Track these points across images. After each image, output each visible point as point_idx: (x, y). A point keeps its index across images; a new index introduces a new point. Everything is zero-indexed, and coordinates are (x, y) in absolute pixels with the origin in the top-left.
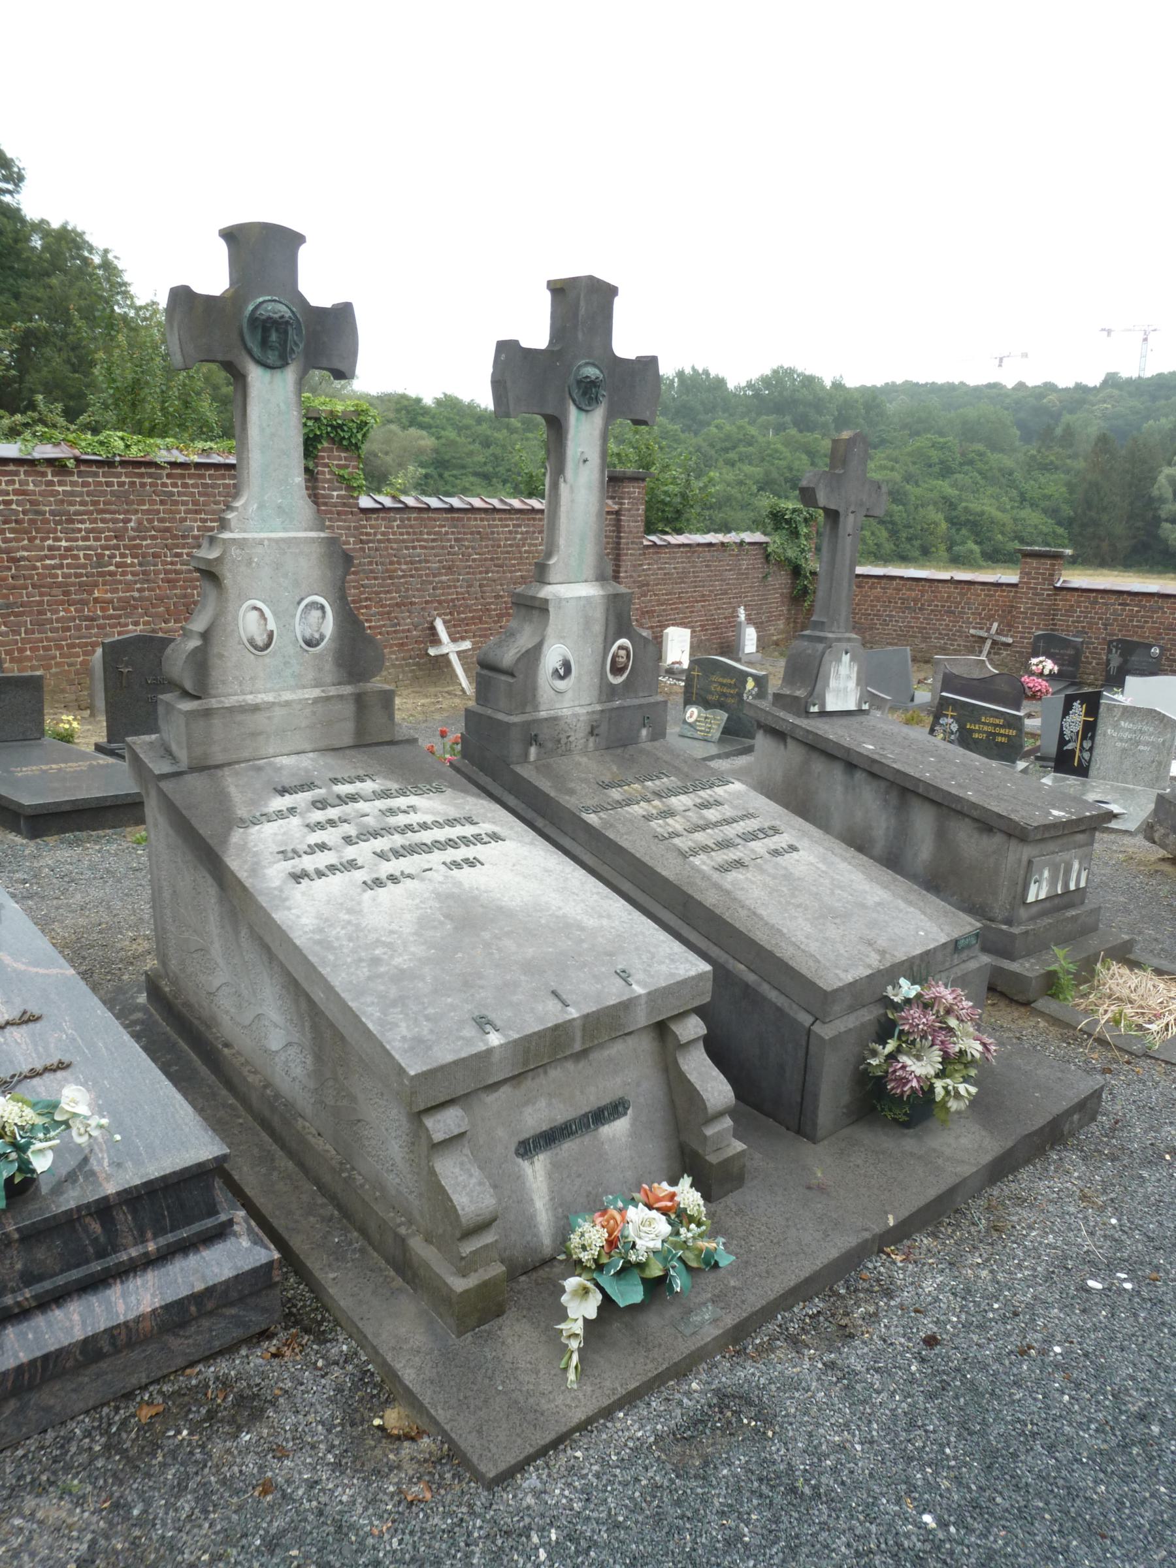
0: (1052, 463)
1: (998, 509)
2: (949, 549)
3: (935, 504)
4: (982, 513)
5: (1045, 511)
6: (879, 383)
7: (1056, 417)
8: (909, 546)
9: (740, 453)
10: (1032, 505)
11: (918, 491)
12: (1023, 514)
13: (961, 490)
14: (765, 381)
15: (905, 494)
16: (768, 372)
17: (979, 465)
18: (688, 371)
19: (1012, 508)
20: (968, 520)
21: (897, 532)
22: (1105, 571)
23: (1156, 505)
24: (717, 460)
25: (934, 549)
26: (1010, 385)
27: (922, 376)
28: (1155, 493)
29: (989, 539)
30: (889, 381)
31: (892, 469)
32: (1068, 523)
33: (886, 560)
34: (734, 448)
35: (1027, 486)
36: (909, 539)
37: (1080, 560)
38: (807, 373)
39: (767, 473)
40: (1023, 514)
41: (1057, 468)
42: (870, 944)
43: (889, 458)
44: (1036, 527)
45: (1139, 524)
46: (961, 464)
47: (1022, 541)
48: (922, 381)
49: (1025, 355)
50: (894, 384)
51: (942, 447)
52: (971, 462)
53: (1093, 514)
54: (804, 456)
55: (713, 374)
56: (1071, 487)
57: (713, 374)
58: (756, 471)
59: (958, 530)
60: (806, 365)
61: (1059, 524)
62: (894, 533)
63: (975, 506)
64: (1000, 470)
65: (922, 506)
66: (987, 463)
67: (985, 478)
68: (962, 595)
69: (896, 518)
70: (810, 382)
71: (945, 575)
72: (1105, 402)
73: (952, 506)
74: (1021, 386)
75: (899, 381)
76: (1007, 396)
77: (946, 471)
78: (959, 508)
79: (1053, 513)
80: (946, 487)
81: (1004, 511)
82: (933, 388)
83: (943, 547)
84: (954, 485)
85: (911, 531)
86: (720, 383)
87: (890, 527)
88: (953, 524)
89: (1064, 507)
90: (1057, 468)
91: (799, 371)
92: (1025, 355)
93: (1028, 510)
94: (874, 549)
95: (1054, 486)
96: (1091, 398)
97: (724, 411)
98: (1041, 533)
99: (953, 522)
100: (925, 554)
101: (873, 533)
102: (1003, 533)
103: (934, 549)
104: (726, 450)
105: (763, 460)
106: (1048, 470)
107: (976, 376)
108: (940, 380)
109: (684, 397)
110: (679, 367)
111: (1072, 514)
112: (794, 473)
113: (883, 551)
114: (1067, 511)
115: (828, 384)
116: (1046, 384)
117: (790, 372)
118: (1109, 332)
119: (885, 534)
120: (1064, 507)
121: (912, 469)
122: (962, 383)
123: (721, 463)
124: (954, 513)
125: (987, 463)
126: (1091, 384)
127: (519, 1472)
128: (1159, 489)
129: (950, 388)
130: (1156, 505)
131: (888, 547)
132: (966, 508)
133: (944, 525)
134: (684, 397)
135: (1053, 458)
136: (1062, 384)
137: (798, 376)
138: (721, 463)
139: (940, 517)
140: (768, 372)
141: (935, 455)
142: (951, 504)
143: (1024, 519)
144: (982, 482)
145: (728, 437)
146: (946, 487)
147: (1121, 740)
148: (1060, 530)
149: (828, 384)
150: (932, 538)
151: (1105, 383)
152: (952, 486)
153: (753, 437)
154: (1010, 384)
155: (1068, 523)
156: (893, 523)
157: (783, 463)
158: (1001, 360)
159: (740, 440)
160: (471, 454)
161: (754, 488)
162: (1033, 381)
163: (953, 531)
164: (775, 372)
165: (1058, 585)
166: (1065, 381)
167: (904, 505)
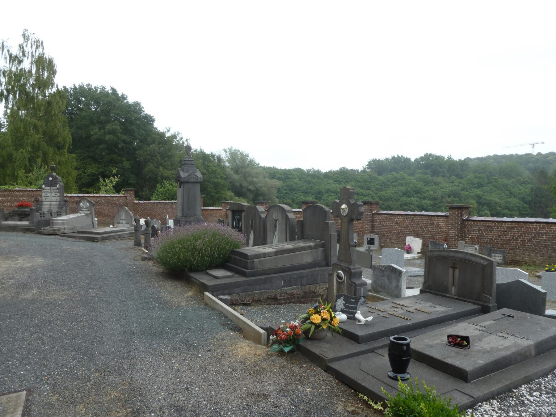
0: (527, 181)
1: (499, 198)
4: (492, 200)
5: (520, 199)
12: (510, 200)
14: (422, 158)
17: (494, 183)
18: (396, 156)
27: (500, 152)
29: (495, 209)
32: (529, 203)
42: (206, 304)
44: (515, 204)
46: (487, 183)
47: (509, 209)
49: (543, 143)
50: (489, 156)
52: (491, 182)
57: (234, 149)
59: (482, 207)
60: (496, 154)
61: (525, 203)
70: (438, 158)
73: (480, 198)
74: (539, 154)
75: (492, 155)
77: (480, 186)
79: (523, 199)
90: (529, 183)
92: (543, 143)
95: (525, 190)
98: (517, 206)
102: (500, 207)
104: (395, 182)
107: (522, 151)
117: (430, 155)
120: (526, 197)
123: (391, 186)
124: (481, 200)
127: (470, 408)
132: (485, 199)
138: (391, 186)
146: (478, 192)
148: (525, 205)
149: (446, 158)
155: (529, 203)
158: (533, 145)
160: (303, 186)
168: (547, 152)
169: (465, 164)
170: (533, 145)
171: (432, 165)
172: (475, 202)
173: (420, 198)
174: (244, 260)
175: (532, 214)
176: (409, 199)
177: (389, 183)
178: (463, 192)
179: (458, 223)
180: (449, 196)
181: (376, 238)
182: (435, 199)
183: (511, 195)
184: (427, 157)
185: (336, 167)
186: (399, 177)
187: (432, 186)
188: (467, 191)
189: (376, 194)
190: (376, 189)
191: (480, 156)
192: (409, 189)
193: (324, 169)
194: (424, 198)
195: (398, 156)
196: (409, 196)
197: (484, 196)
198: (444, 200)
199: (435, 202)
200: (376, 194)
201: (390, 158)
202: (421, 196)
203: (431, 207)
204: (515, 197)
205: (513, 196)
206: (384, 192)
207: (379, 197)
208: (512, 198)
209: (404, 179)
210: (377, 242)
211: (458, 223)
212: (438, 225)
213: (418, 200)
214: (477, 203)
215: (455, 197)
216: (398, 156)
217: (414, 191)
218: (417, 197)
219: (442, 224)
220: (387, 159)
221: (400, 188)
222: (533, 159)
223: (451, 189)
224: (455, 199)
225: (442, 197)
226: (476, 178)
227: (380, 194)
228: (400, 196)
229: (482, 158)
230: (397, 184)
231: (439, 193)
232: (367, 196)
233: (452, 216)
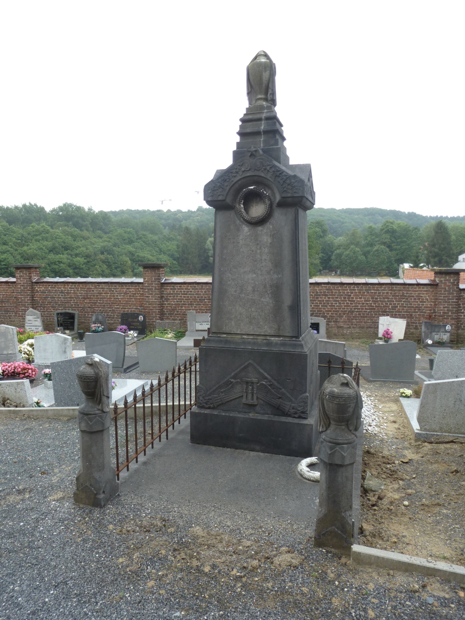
0: (172, 238)
2: (133, 271)
3: (126, 254)
4: (144, 257)
5: (169, 255)
6: (117, 210)
7: (180, 221)
8: (116, 271)
9: (43, 237)
10: (164, 253)
11: (119, 250)
12: (161, 257)
13: (136, 248)
14: (61, 209)
15: (113, 250)
16: (62, 205)
17: (144, 239)
18: (28, 204)
19: (157, 254)
20: (139, 260)
21: (111, 266)
22: (192, 276)
23: (207, 251)
24: (32, 240)
25: (126, 271)
26: (165, 211)
28: (206, 247)
30: (121, 209)
31: (109, 242)
33: (106, 276)
34: (40, 234)
35: (162, 246)
36: (116, 268)
37: (183, 272)
38: (78, 205)
39: (54, 244)
40: (161, 257)
41: (173, 240)
43: (108, 237)
45: (203, 258)
46: (137, 239)
48: (133, 209)
49: (170, 200)
50: (123, 210)
51: (129, 233)
52: (140, 238)
53: (186, 255)
54: (70, 237)
55: (39, 206)
56: (178, 246)
57: (39, 206)
58: (50, 244)
61: (174, 260)
62: (109, 266)
63: (142, 254)
64: (152, 241)
65: (121, 255)
66: (146, 238)
67: (146, 244)
68: (96, 288)
69: (110, 260)
70: (79, 209)
71: (337, 280)
72: (198, 216)
73: (133, 255)
74: (169, 211)
75: (125, 209)
76: (164, 214)
77: (131, 242)
78: (136, 255)
79: (172, 256)
80: (130, 248)
81: (153, 256)
82: (138, 212)
83: (130, 270)
84: (134, 247)
85: (116, 265)
86: (42, 209)
87: (108, 264)
88: (134, 261)
89: (175, 253)
91: (74, 204)
92: (170, 200)
93: (162, 255)
94: (101, 272)
95: (172, 246)
96: (193, 215)
97: (44, 220)
99: (133, 260)
100: (123, 273)
101: (100, 267)
103: (126, 271)
104: (37, 235)
105: (52, 240)
106: (171, 240)
107: (153, 208)
108: (140, 209)
109: (26, 215)
110: (23, 203)
111: (178, 256)
112: (66, 244)
113: (105, 273)
114: (177, 255)
115: (86, 209)
116: (178, 210)
117: (71, 205)
118: (198, 192)
119: (105, 266)
120: (175, 253)
121: (117, 241)
122: (148, 210)
123: (33, 241)
124: (134, 257)
125: (146, 238)
126: (193, 210)
128: (207, 246)
129: (144, 211)
130: (207, 251)
131: (107, 271)
132: (138, 255)
133: (130, 262)
134: (26, 215)
135: (172, 236)
136: (184, 211)
137: (74, 206)
138: (33, 241)
139: (128, 259)
140: (62, 205)
141: (126, 236)
142: (132, 254)
143: (161, 259)
144: (145, 245)
145: (37, 230)
146: (130, 248)
147: (356, 333)
148: (175, 262)
149: (5, 207)
150: (125, 267)
151: (198, 210)
152: (132, 247)
153: (48, 230)
154: (165, 211)
156: (109, 262)
157: (61, 240)
158: (162, 202)
159: (43, 231)
161: (47, 251)
162: (173, 209)
163: (134, 264)
164: (65, 205)
165: (163, 282)
166: (185, 209)
167: (113, 255)
168: (175, 210)
169: (104, 218)
170: (162, 202)
171: (73, 217)
172: (128, 259)
173: (71, 255)
174: (296, 421)
175: (180, 271)
176: (58, 257)
177: (30, 237)
178: (114, 248)
179: (453, 294)
180: (102, 253)
181: (323, 323)
182: (87, 256)
183: (161, 251)
184: (66, 208)
185: (363, 207)
186: (42, 229)
187: (81, 241)
188: (119, 247)
189: (16, 250)
190: (15, 244)
191: (113, 210)
192: (57, 245)
193: (338, 208)
194: (77, 255)
195: (30, 203)
196: (57, 253)
197: (136, 252)
198: (98, 257)
199: (88, 259)
200: (16, 250)
201: (21, 206)
202: (72, 253)
203: (84, 266)
204: (164, 253)
205: (162, 253)
206: (25, 248)
207: (20, 254)
208: (162, 255)
209: (48, 232)
210: (323, 329)
211: (453, 294)
212: (419, 297)
213: (69, 257)
214: (130, 259)
215: (108, 254)
216: (30, 203)
217: (62, 247)
218: (68, 254)
219: (425, 296)
220: (16, 207)
221: (46, 243)
222: (164, 216)
223: (102, 244)
224: (108, 256)
225: (95, 254)
226: (125, 232)
227: (21, 250)
228: (46, 253)
229: (115, 212)
230: (41, 238)
231: (91, 250)
232: (4, 253)
233: (445, 284)
